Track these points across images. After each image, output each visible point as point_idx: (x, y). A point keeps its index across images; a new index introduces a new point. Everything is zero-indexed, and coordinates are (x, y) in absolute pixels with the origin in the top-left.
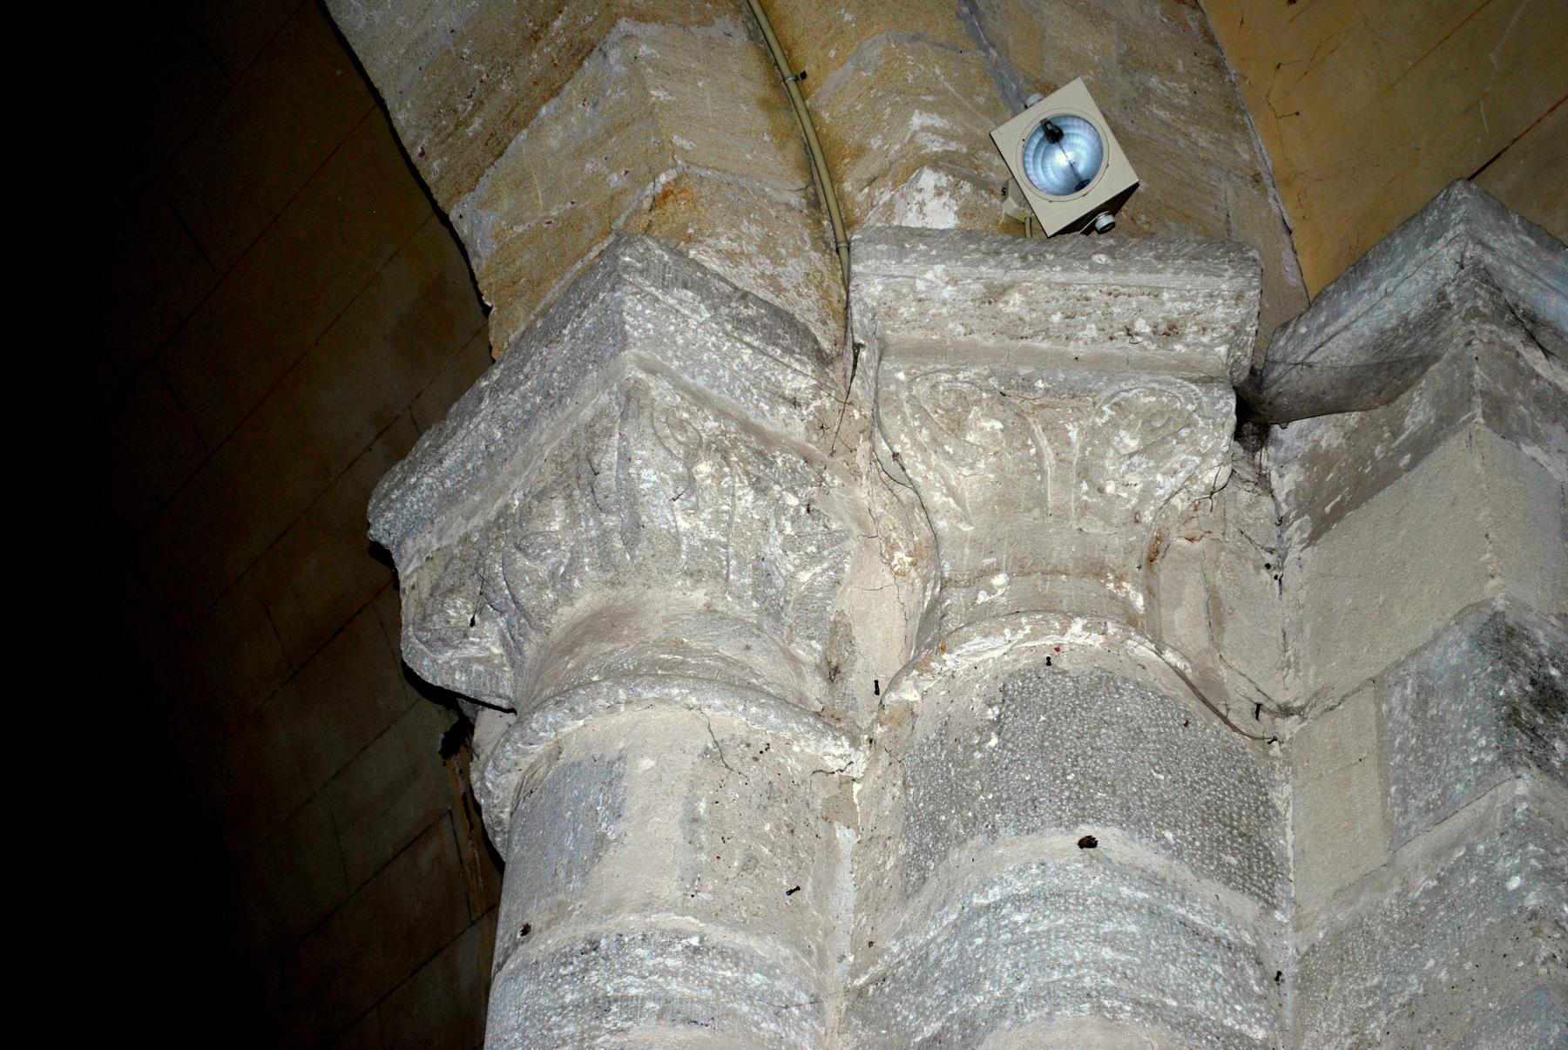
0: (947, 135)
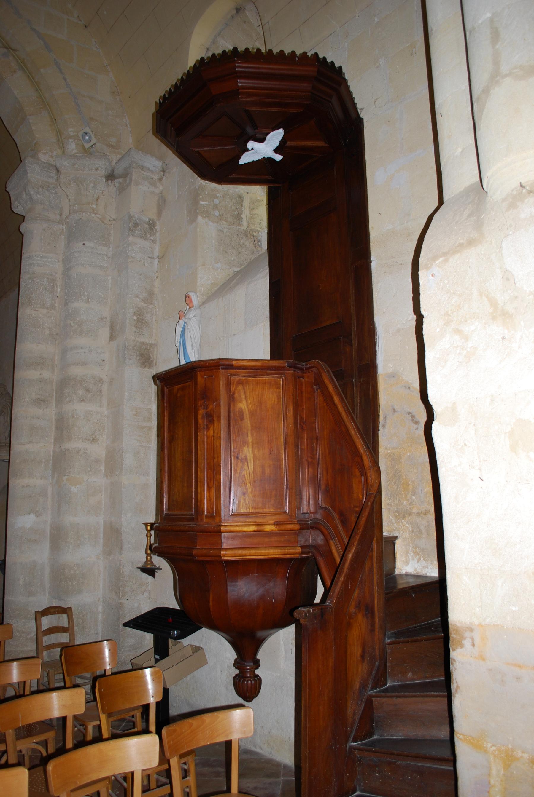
0: (73, 132)
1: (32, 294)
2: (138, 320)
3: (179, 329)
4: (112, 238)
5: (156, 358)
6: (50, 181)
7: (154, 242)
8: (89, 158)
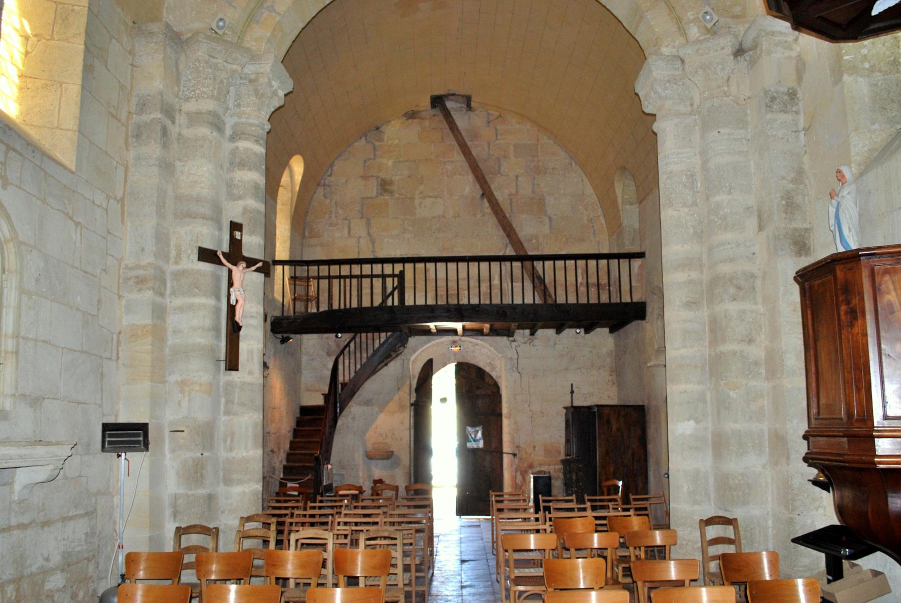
2: (787, 205)
3: (832, 211)
4: (749, 119)
5: (410, 394)
6: (677, 73)
7: (797, 113)
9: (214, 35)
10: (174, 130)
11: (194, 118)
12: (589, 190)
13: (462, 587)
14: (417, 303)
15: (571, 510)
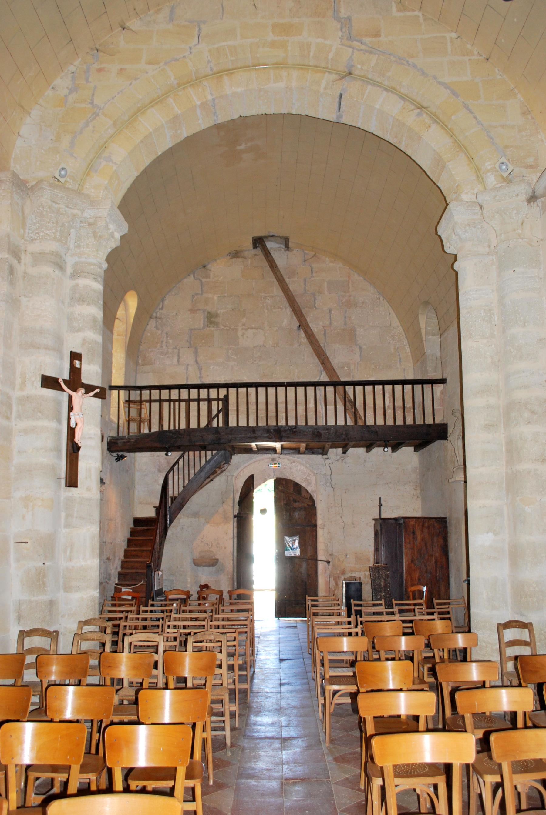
1: (472, 327)
5: (234, 507)
8: (508, 187)
9: (57, 183)
10: (20, 269)
11: (39, 258)
12: (396, 322)
13: (281, 684)
14: (240, 425)
15: (381, 614)
